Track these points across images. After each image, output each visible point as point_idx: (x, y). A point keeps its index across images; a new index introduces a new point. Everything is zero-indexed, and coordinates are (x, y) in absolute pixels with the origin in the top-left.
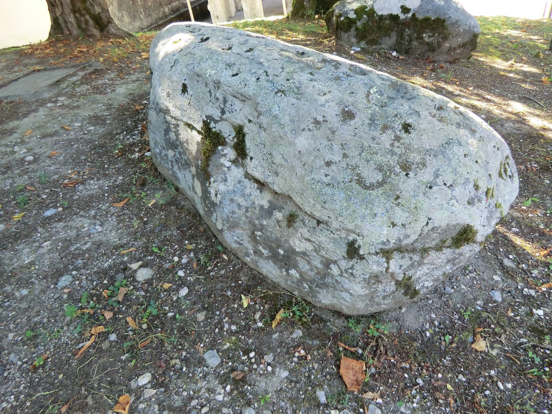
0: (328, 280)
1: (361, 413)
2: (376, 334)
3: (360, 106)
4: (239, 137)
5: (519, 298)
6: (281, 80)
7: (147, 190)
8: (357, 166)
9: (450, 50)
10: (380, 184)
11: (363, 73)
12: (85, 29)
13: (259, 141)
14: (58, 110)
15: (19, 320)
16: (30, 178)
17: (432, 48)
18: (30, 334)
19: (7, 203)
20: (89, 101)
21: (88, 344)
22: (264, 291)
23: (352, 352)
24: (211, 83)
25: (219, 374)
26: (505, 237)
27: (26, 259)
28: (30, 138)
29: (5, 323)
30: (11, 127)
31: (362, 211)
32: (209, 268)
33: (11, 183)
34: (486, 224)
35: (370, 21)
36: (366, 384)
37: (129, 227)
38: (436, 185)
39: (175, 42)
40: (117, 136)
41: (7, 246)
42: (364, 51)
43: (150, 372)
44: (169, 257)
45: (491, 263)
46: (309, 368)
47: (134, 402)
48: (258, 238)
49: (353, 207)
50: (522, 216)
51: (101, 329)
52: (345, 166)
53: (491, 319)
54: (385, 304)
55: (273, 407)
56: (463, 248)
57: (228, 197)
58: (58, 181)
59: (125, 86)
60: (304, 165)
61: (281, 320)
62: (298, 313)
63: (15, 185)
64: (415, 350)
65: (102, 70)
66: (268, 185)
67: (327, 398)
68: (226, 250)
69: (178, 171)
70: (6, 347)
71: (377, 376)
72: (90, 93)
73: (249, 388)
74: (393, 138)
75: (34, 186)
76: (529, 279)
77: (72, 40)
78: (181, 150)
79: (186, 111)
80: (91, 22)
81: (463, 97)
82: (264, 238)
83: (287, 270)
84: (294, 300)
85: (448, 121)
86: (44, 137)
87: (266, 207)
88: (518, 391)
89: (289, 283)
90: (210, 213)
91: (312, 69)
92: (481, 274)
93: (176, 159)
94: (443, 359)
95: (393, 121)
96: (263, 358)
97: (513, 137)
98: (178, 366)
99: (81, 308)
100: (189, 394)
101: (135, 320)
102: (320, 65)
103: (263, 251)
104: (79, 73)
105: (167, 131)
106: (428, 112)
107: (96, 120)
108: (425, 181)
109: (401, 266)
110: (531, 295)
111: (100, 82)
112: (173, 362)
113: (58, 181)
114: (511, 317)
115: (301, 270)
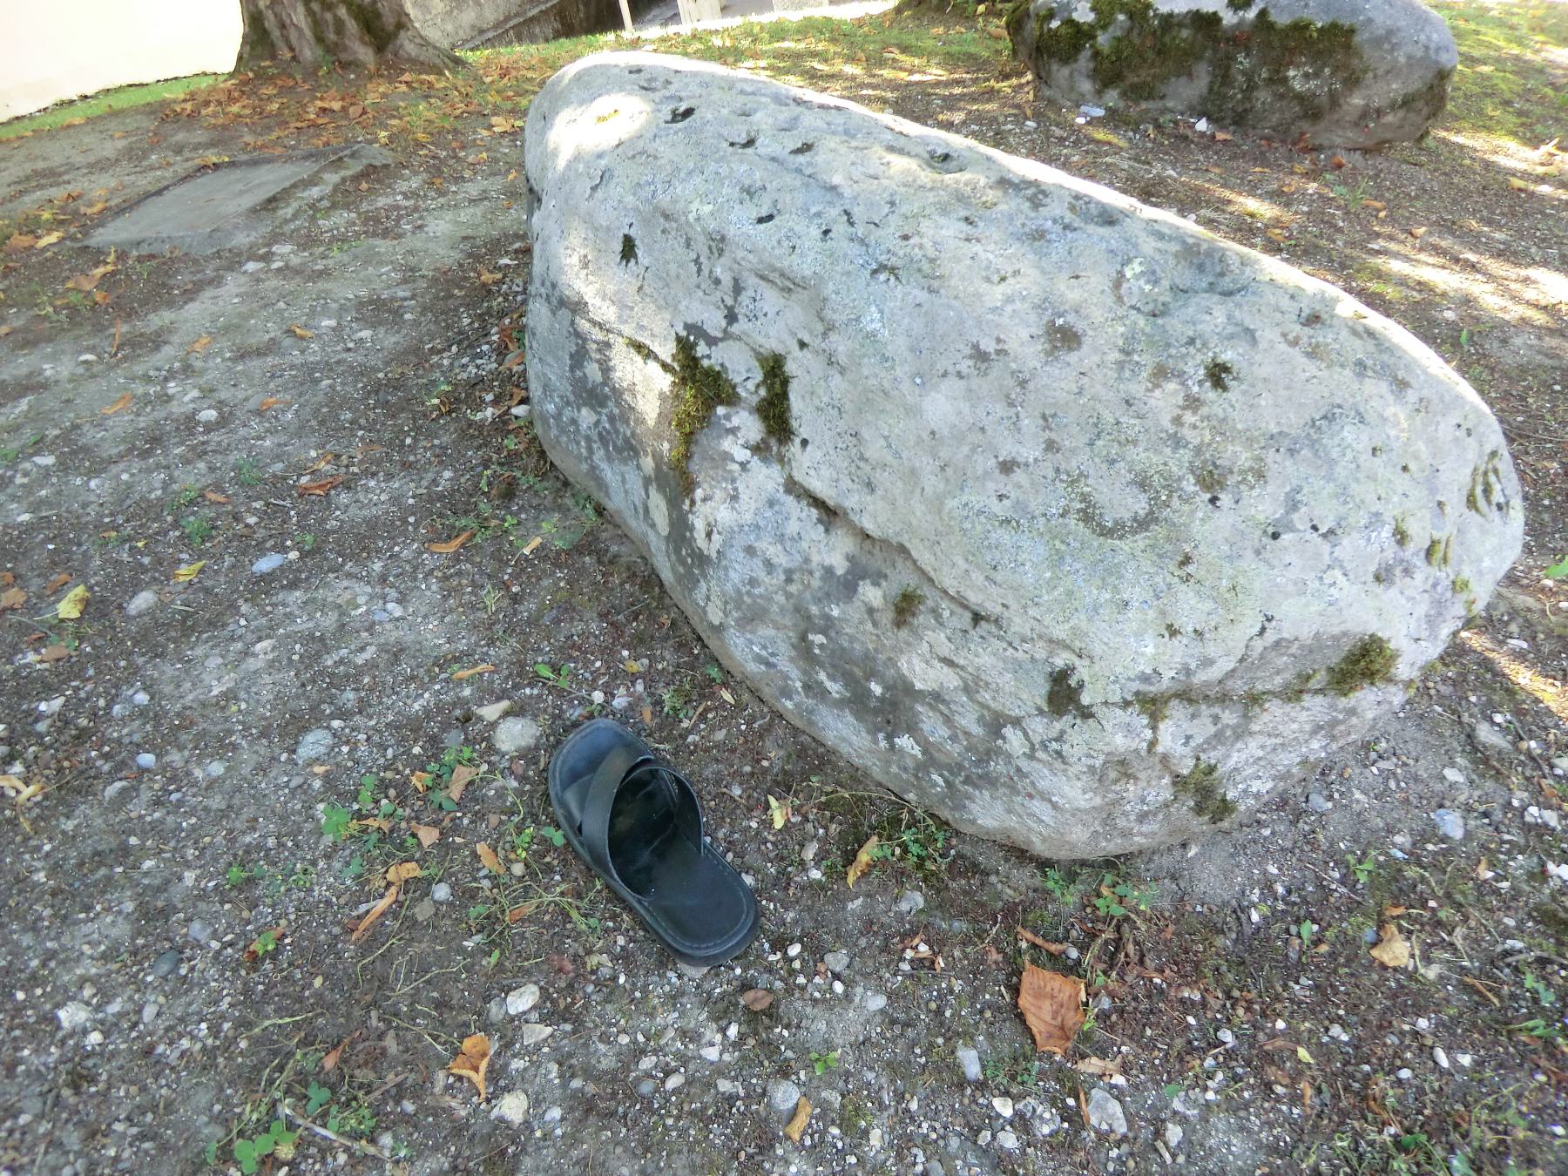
0: (997, 767)
1: (1070, 1108)
2: (1118, 911)
3: (1098, 315)
4: (773, 384)
5: (1514, 831)
6: (887, 237)
7: (522, 509)
8: (1081, 474)
9: (1365, 114)
10: (1143, 524)
11: (1109, 218)
12: (336, 44)
13: (825, 399)
14: (274, 283)
15: (207, 839)
16: (212, 469)
17: (1312, 110)
18: (236, 873)
19: (157, 533)
20: (356, 257)
21: (382, 905)
22: (829, 789)
23: (1051, 954)
24: (702, 239)
25: (709, 994)
26: (1487, 664)
27: (214, 683)
28: (206, 359)
29: (173, 843)
30: (154, 328)
31: (1092, 593)
32: (686, 724)
33: (164, 482)
34: (1424, 634)
35: (1136, 32)
36: (1086, 1037)
37: (473, 607)
38: (1291, 528)
39: (602, 119)
40: (435, 359)
41: (165, 647)
42: (1113, 119)
43: (536, 983)
44: (579, 690)
45: (1441, 735)
46: (938, 991)
47: (498, 1054)
48: (817, 651)
49: (1068, 582)
50: (1539, 606)
51: (411, 870)
52: (1051, 474)
53: (1429, 885)
54: (1142, 834)
55: (846, 1082)
56: (1358, 694)
57: (740, 541)
58: (285, 478)
59: (449, 216)
60: (942, 469)
61: (872, 866)
62: (915, 849)
63: (175, 487)
64: (1218, 955)
65: (386, 166)
66: (846, 514)
67: (984, 1068)
68: (729, 678)
69: (604, 465)
70: (180, 906)
71: (1114, 1018)
72: (357, 235)
73: (786, 1033)
74: (1181, 403)
75: (224, 491)
76: (1544, 782)
77: (299, 77)
78: (616, 411)
79: (632, 309)
80: (352, 26)
81: (1396, 255)
82: (833, 652)
83: (890, 738)
84: (905, 816)
85: (1334, 356)
86: (242, 357)
87: (840, 572)
88: (1488, 1073)
89: (894, 769)
90: (689, 581)
91: (971, 215)
92: (1411, 762)
93: (600, 434)
94: (1291, 984)
95: (1183, 357)
96: (822, 960)
97: (1535, 377)
98: (606, 972)
99: (359, 815)
100: (635, 1042)
101: (495, 850)
102: (991, 195)
103: (829, 685)
104: (326, 176)
105: (579, 358)
106: (1278, 331)
107: (378, 311)
108: (1261, 517)
109: (1188, 738)
110: (1546, 825)
111: (382, 202)
112: (593, 961)
113: (285, 478)
114: (1485, 881)
115: (926, 739)
